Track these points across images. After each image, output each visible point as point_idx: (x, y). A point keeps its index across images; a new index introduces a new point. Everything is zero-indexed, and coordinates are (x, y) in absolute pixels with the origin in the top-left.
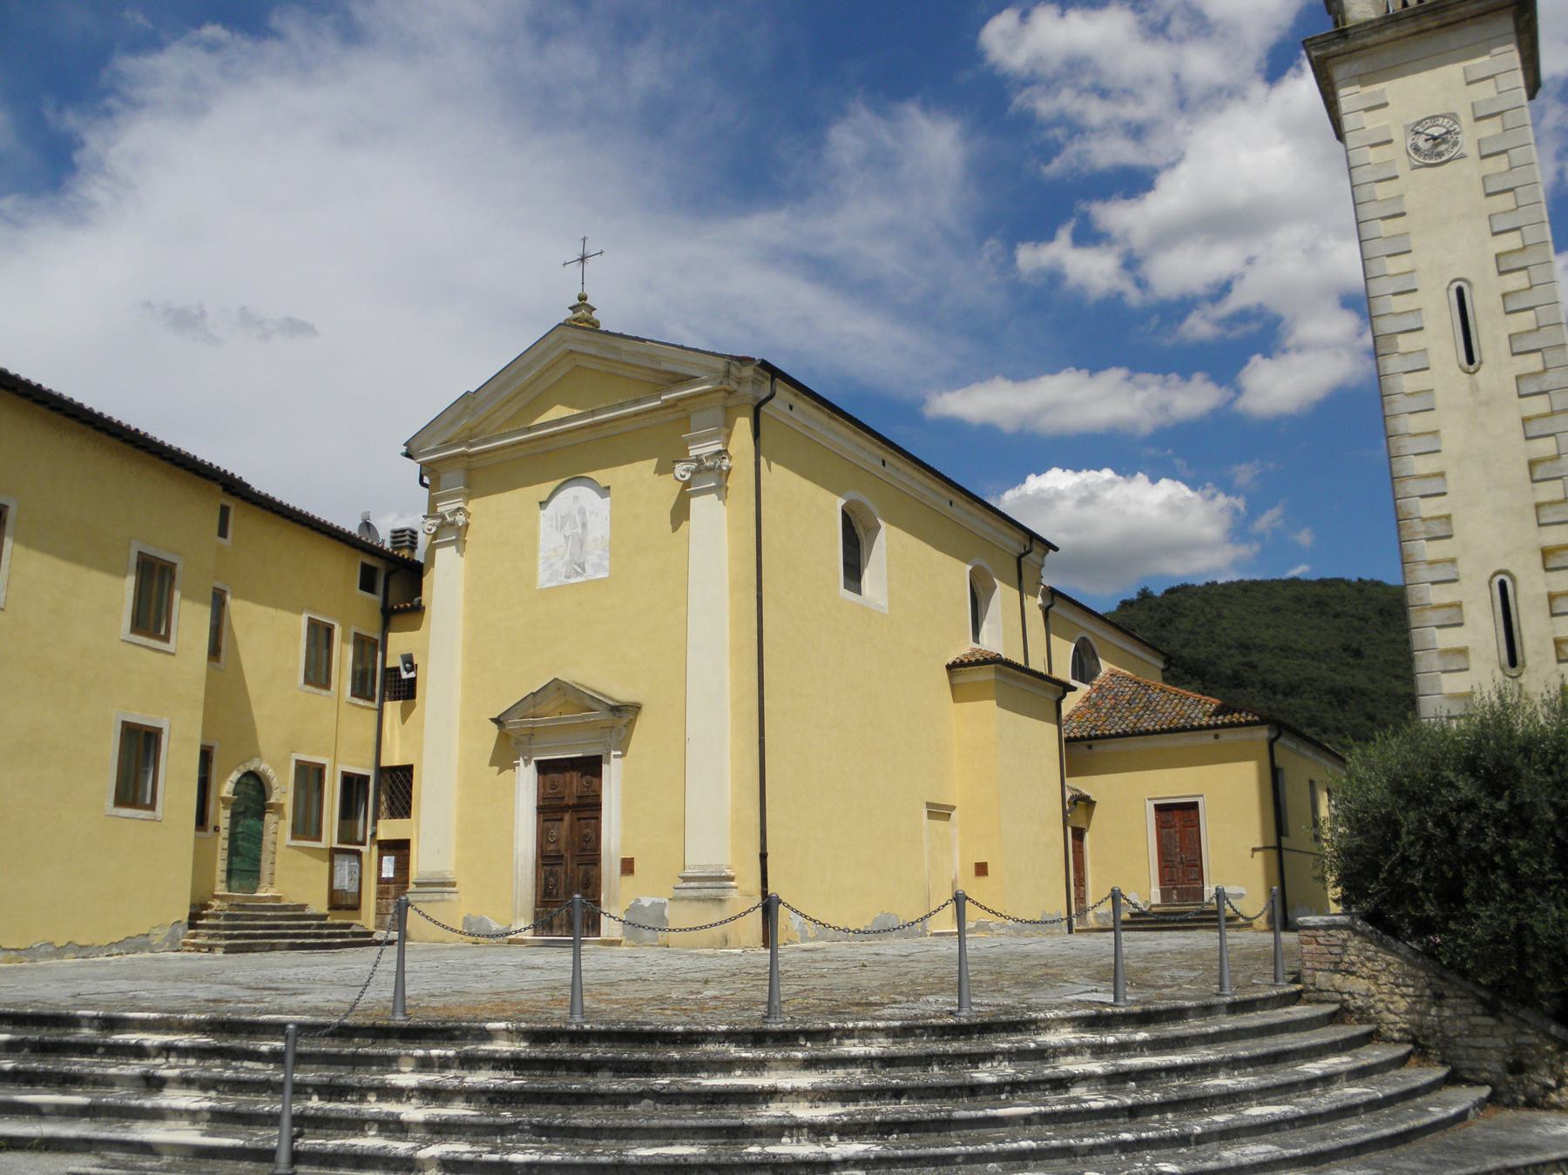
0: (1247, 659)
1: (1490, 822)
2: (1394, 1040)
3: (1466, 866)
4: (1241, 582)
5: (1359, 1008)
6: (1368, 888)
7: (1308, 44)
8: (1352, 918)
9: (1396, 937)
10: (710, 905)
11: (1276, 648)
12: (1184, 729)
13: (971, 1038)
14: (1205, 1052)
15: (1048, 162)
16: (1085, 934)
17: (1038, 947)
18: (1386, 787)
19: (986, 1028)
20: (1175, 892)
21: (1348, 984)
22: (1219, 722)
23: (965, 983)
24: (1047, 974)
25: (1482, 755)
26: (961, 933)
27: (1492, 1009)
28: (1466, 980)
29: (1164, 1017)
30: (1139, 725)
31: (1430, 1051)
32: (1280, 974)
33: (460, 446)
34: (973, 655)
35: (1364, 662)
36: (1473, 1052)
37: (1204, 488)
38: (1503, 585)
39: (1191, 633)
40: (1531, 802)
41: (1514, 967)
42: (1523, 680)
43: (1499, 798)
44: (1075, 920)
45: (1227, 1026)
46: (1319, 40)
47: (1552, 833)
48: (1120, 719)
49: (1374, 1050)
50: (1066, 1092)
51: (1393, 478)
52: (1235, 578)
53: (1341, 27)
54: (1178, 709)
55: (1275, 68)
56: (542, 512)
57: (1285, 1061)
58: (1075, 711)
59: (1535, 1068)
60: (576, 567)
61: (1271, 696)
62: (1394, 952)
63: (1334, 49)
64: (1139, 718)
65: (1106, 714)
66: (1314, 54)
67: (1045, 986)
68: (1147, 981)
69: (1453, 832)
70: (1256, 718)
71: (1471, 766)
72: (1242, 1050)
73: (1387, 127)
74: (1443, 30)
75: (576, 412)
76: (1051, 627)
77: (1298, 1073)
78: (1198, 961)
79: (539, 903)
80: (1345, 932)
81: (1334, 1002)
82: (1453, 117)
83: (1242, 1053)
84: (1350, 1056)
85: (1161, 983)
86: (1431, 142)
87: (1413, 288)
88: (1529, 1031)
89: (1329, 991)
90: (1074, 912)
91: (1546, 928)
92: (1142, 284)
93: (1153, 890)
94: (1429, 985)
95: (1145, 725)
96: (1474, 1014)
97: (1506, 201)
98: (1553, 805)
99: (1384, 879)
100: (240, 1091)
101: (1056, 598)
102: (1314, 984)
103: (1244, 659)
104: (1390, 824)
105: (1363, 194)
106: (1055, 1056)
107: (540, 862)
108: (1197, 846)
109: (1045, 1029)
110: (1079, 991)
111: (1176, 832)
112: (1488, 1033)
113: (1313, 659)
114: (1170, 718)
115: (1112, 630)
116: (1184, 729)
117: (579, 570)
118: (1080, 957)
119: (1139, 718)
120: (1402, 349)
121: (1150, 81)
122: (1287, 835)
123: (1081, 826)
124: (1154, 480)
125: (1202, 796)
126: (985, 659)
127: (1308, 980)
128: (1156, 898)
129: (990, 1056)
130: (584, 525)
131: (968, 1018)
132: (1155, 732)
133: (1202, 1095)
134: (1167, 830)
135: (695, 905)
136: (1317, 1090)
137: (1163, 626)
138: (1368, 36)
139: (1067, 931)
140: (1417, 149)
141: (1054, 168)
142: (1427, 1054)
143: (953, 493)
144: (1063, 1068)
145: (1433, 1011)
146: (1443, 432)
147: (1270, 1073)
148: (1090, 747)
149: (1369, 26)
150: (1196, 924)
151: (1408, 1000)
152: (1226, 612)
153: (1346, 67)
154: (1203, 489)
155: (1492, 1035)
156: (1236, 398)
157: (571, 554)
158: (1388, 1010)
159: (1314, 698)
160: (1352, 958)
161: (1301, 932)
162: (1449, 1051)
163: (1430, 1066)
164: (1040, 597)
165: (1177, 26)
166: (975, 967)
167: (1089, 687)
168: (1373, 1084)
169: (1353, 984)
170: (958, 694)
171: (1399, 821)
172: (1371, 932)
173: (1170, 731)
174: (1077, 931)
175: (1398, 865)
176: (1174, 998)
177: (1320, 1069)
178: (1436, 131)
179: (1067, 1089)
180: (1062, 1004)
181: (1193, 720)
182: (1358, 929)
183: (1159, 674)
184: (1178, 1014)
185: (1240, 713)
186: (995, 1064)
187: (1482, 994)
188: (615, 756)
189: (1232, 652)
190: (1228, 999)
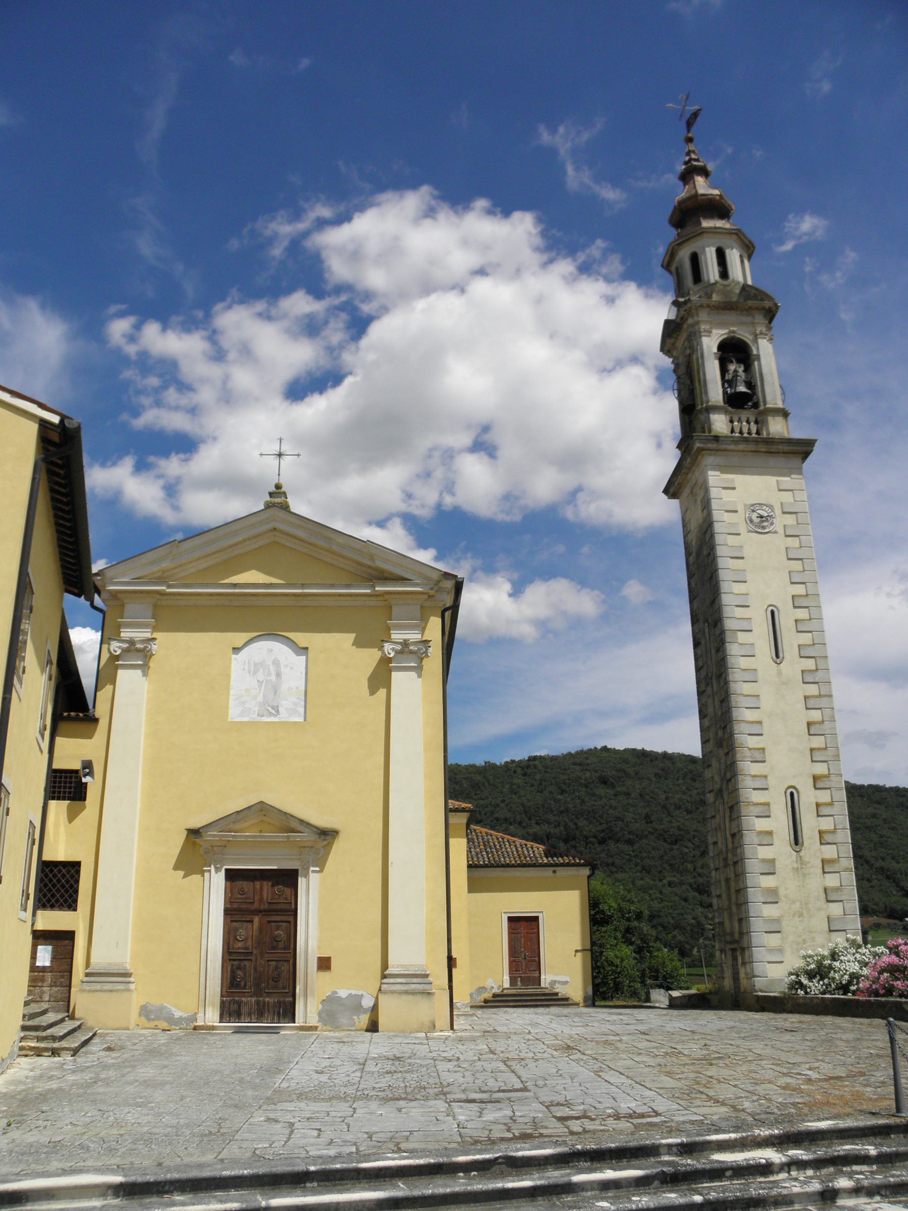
10: (419, 997)
33: (162, 586)
38: (792, 794)
42: (802, 854)
56: (234, 656)
60: (270, 709)
63: (710, 445)
73: (735, 502)
75: (282, 582)
79: (225, 993)
82: (771, 507)
86: (759, 519)
93: (505, 977)
100: (899, 1193)
117: (273, 711)
120: (740, 641)
125: (542, 912)
128: (507, 984)
130: (278, 675)
135: (405, 997)
138: (730, 444)
140: (751, 521)
146: (762, 697)
157: (264, 696)
188: (313, 871)
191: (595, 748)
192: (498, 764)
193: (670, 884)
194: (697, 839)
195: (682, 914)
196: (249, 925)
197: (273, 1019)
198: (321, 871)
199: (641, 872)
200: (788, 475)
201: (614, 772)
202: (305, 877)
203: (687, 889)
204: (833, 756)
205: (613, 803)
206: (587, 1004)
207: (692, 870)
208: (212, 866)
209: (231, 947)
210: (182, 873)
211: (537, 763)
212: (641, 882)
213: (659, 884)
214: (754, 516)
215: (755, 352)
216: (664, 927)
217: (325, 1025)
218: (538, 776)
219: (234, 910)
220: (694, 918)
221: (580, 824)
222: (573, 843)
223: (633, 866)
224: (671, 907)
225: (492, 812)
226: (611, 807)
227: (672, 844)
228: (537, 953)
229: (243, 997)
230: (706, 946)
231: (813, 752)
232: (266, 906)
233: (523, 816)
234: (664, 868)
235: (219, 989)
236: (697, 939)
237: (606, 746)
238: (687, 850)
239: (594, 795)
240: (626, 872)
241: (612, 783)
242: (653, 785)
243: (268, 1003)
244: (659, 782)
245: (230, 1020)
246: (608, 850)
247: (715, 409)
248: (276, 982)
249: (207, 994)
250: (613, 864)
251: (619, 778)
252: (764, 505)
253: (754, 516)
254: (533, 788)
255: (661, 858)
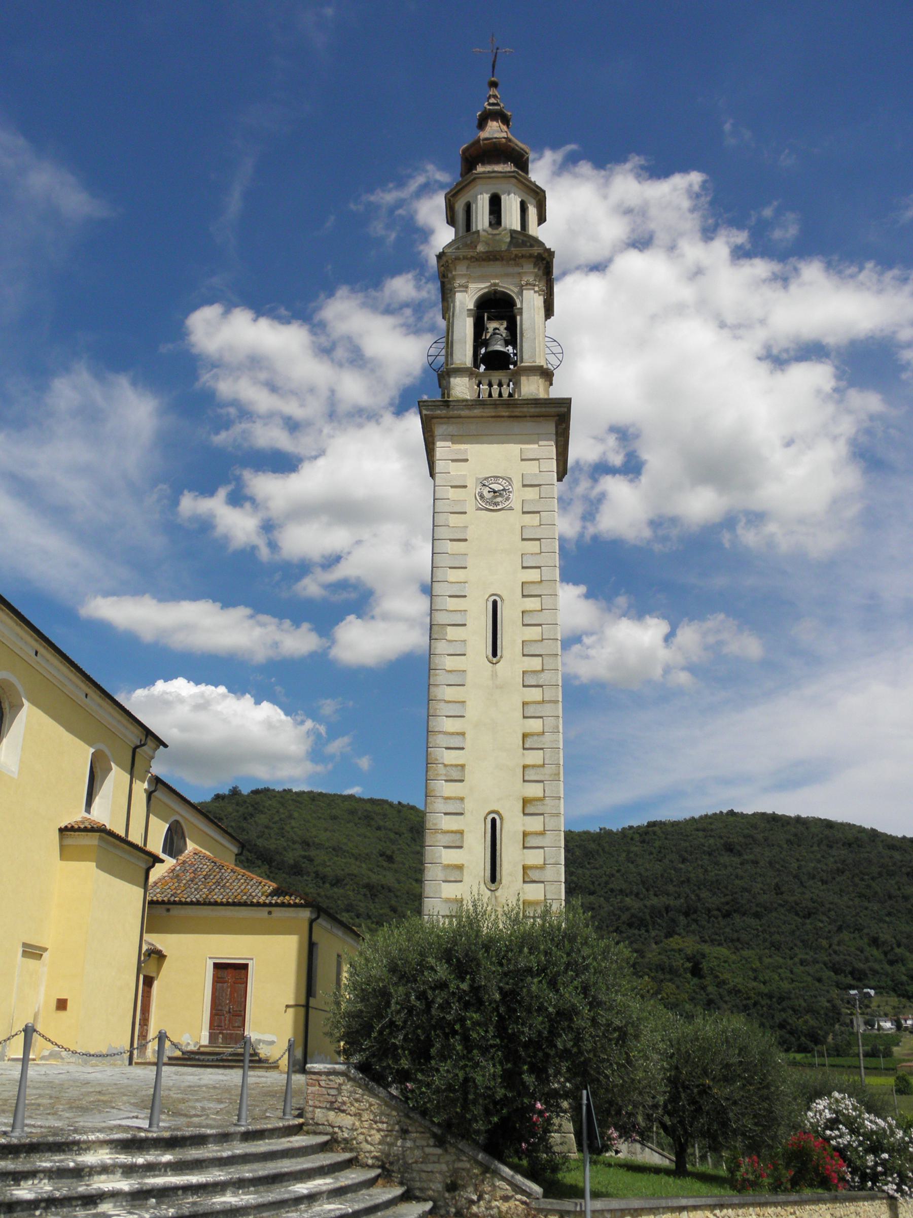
0: (306, 854)
1: (455, 999)
2: (367, 1165)
3: (435, 1031)
4: (311, 792)
5: (345, 1139)
6: (362, 1044)
7: (421, 405)
8: (348, 1067)
9: (379, 1085)
11: (330, 847)
12: (245, 904)
13: (18, 1157)
14: (218, 1173)
15: (217, 433)
16: (143, 1067)
17: (99, 1076)
18: (385, 966)
19: (33, 1148)
20: (221, 1036)
21: (339, 1119)
22: (273, 902)
23: (21, 1107)
24: (99, 1101)
25: (456, 948)
26: (25, 1061)
27: (440, 1142)
28: (425, 1119)
29: (188, 1142)
30: (210, 896)
31: (393, 1174)
32: (288, 1110)
34: (82, 822)
35: (395, 866)
36: (424, 1175)
37: (297, 714)
38: (494, 821)
39: (267, 827)
40: (485, 985)
41: (458, 1110)
42: (498, 893)
43: (463, 980)
44: (135, 1052)
45: (238, 1152)
46: (430, 404)
47: (497, 1009)
48: (196, 890)
49: (352, 1173)
50: (95, 1208)
51: (428, 732)
52: (306, 789)
53: (446, 399)
54: (243, 887)
55: (400, 410)
57: (281, 1182)
58: (160, 879)
59: (464, 1187)
61: (321, 885)
62: (376, 1096)
63: (439, 412)
64: (211, 891)
65: (185, 884)
66: (424, 412)
67: (95, 1111)
68: (182, 1110)
69: (429, 1005)
70: (302, 901)
71: (447, 955)
72: (247, 1172)
73: (465, 476)
74: (512, 419)
76: (152, 809)
77: (289, 1192)
78: (227, 1095)
80: (341, 1078)
81: (327, 1134)
82: (509, 480)
83: (247, 1175)
84: (333, 1178)
85: (193, 1112)
87: (463, 594)
88: (465, 1159)
89: (323, 1125)
90: (135, 1046)
91: (484, 1081)
92: (273, 546)
93: (203, 1033)
94: (398, 1123)
95: (215, 897)
96: (428, 1146)
97: (533, 547)
98: (500, 989)
99: (375, 1038)
101: (160, 785)
102: (313, 1119)
103: (303, 853)
104: (385, 995)
105: (440, 519)
106: (90, 1175)
108: (243, 999)
109: (85, 1150)
110: (122, 1117)
111: (228, 987)
112: (436, 1160)
113: (356, 859)
114: (235, 894)
115: (200, 817)
116: (245, 904)
118: (131, 1086)
119: (211, 891)
120: (448, 638)
121: (312, 390)
122: (315, 997)
123: (152, 975)
124: (258, 702)
125: (252, 959)
126: (92, 827)
127: (309, 1115)
128: (205, 1041)
129: (32, 1174)
131: (19, 1138)
132: (222, 904)
133: (209, 1211)
134: (221, 985)
136: (302, 1207)
137: (245, 819)
138: (462, 409)
139: (127, 1062)
140: (482, 497)
141: (221, 438)
142: (391, 1176)
143: (89, 687)
144: (95, 1186)
145: (399, 1143)
147: (268, 1192)
148: (168, 910)
149: (464, 403)
150: (234, 1064)
151: (382, 1133)
152: (296, 815)
153: (445, 427)
154: (295, 715)
155: (438, 1162)
156: (330, 647)
158: (367, 1141)
159: (354, 890)
160: (344, 1099)
161: (309, 1077)
162: (406, 1175)
163: (391, 1186)
164: (146, 783)
165: (340, 353)
166: (34, 1092)
167: (174, 861)
168: (346, 1201)
169: (343, 1120)
170: (65, 853)
171: (391, 993)
172: (361, 1079)
173: (234, 904)
174: (137, 1063)
175: (387, 1027)
176: (200, 1126)
177: (307, 1189)
178: (496, 487)
179: (95, 1204)
180: (104, 1128)
181: (253, 898)
182: (352, 1076)
183: (233, 857)
184: (199, 1140)
185: (291, 896)
186: (36, 1182)
187: (435, 1130)
189: (296, 846)
190: (243, 1129)
191: (721, 812)
192: (615, 830)
193: (802, 962)
194: (832, 913)
195: (816, 997)
199: (770, 949)
200: (536, 442)
201: (740, 839)
203: (822, 969)
204: (551, 775)
205: (740, 872)
206: (294, 1069)
207: (827, 946)
211: (656, 829)
212: (769, 960)
213: (790, 962)
214: (485, 492)
215: (519, 306)
216: (794, 1010)
218: (657, 844)
220: (828, 1001)
221: (702, 896)
222: (694, 916)
223: (760, 942)
224: (803, 988)
225: (607, 883)
226: (737, 877)
227: (804, 917)
228: (243, 1006)
230: (842, 1033)
231: (526, 769)
233: (641, 886)
234: (796, 945)
236: (833, 1025)
237: (732, 810)
238: (821, 925)
239: (717, 863)
240: (753, 949)
241: (739, 851)
242: (784, 853)
244: (790, 849)
246: (734, 924)
247: (460, 371)
250: (738, 940)
251: (746, 844)
252: (501, 478)
253: (485, 492)
254: (652, 857)
255: (793, 933)
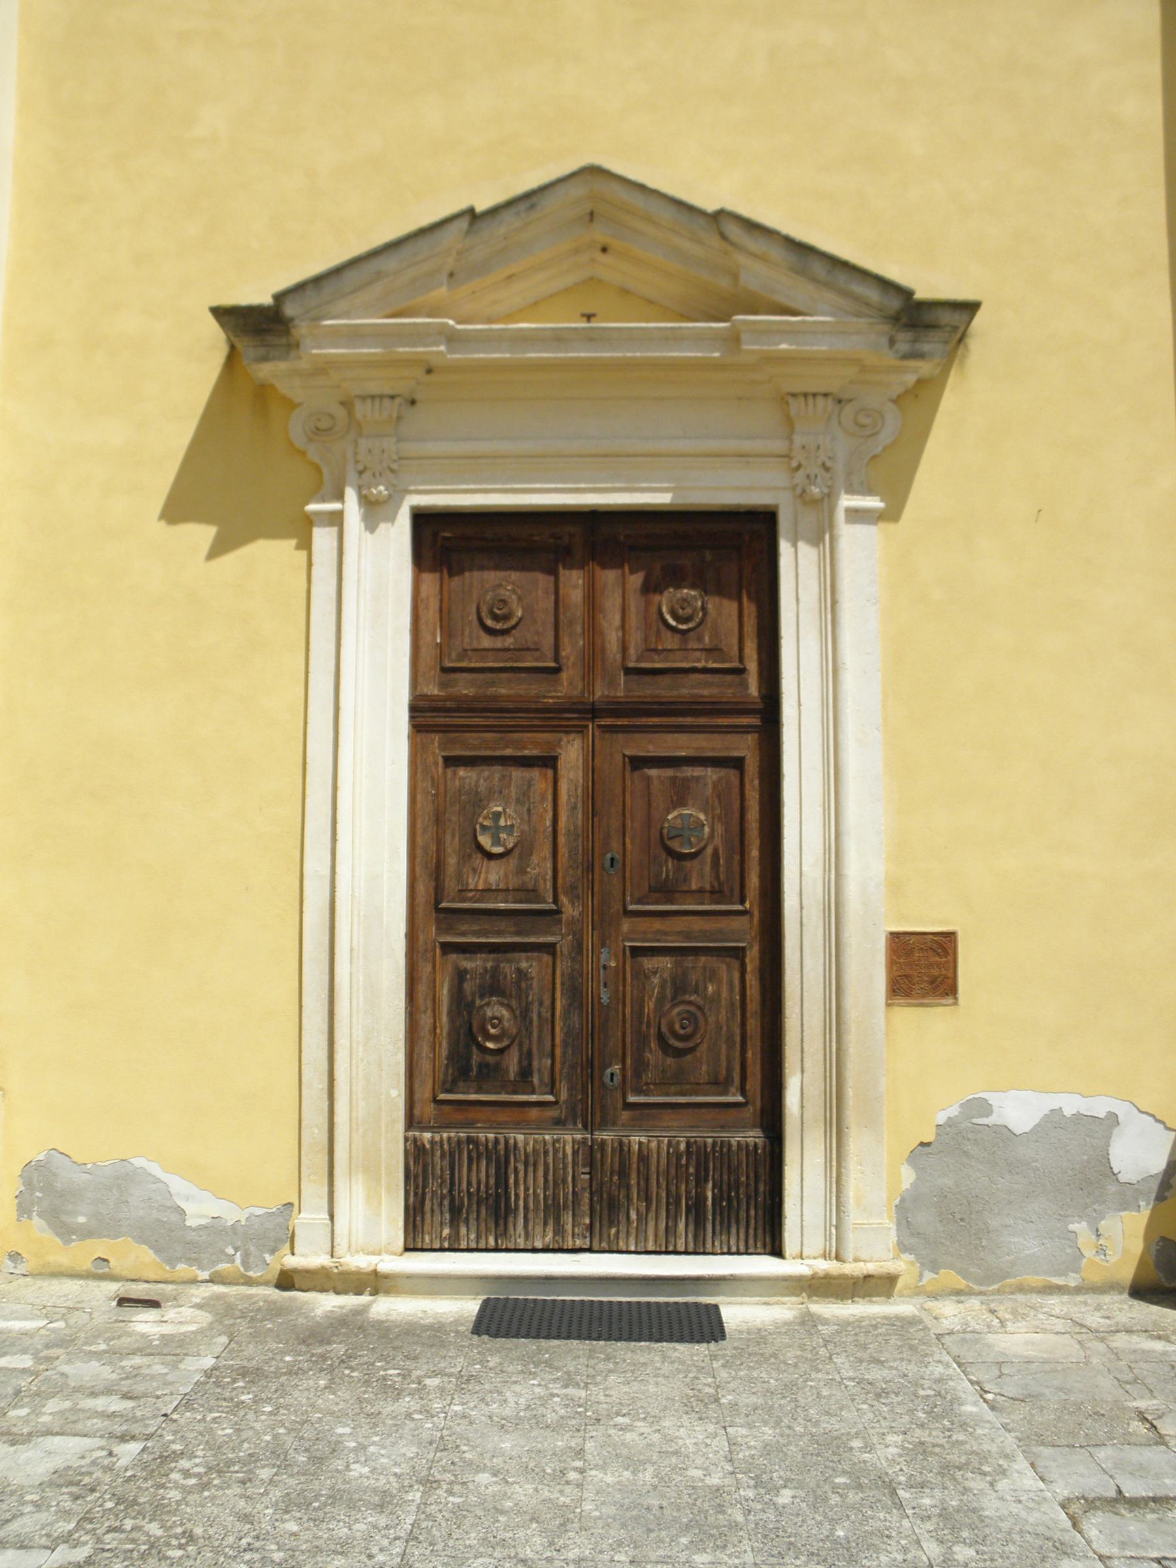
79: (427, 1110)
107: (430, 933)
188: (856, 515)
196: (538, 779)
197: (670, 1231)
198: (891, 514)
202: (816, 540)
208: (351, 494)
209: (451, 885)
210: (204, 534)
217: (935, 1269)
219: (465, 706)
229: (519, 1125)
232: (621, 688)
235: (397, 1094)
243: (644, 1158)
245: (455, 1236)
248: (679, 1053)
249: (341, 1117)
